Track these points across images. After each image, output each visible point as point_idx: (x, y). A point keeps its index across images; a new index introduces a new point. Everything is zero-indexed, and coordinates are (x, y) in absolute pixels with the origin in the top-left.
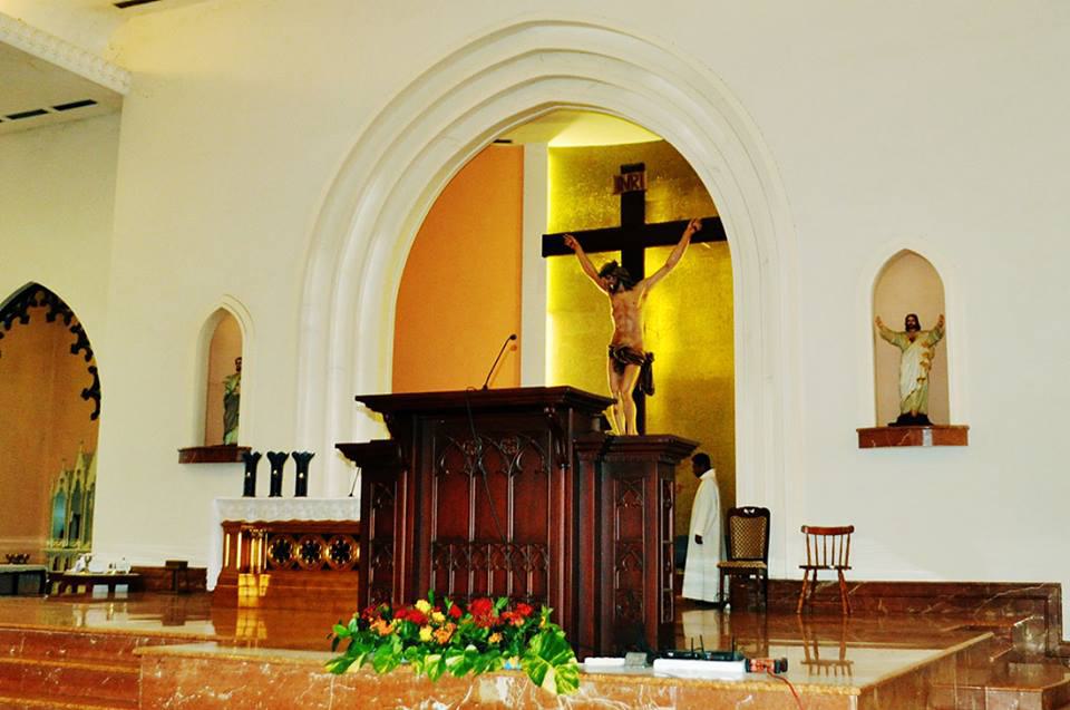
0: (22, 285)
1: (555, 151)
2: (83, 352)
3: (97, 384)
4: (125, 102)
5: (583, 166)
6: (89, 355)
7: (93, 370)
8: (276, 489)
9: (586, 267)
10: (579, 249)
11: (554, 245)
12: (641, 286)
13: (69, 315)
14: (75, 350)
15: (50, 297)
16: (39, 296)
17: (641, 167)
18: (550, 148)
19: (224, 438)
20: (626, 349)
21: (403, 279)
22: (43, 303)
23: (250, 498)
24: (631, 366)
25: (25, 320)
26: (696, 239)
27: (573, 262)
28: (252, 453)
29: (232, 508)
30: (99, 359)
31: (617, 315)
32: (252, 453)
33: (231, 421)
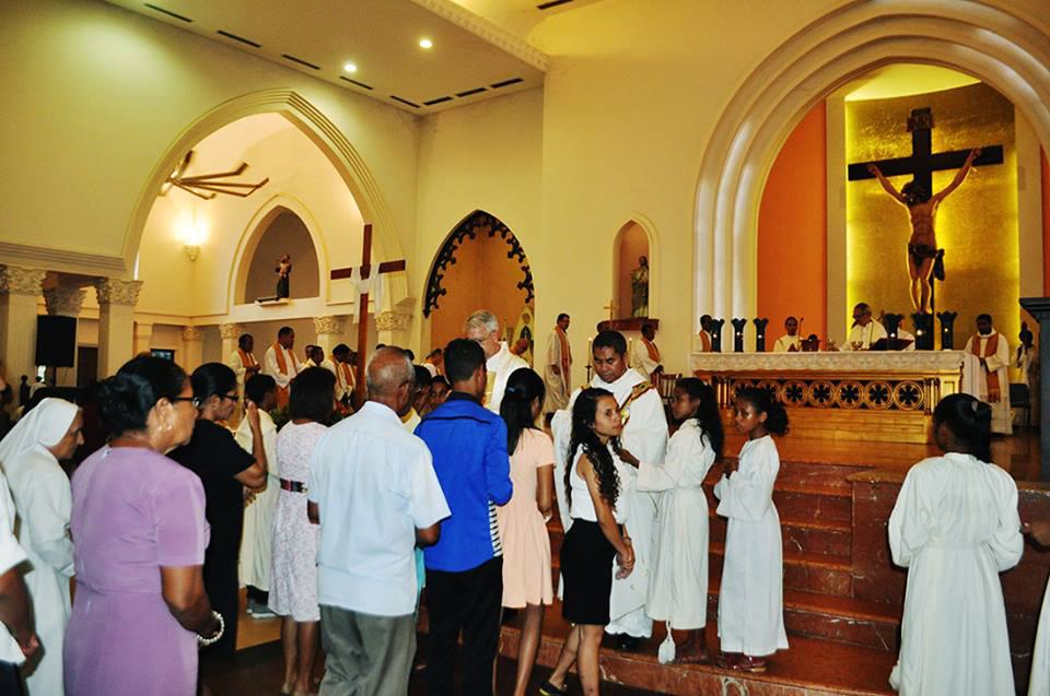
0: (468, 213)
1: (851, 103)
2: (517, 257)
3: (529, 277)
4: (546, 77)
5: (877, 117)
6: (522, 258)
7: (526, 269)
8: (739, 346)
9: (890, 189)
10: (881, 175)
11: (859, 172)
12: (931, 201)
13: (505, 231)
14: (510, 255)
15: (490, 220)
16: (482, 219)
17: (928, 110)
18: (848, 102)
19: (633, 313)
20: (924, 247)
21: (765, 193)
22: (486, 224)
23: (740, 353)
24: (927, 260)
25: (472, 237)
26: (975, 164)
27: (875, 188)
28: (415, 419)
29: (705, 360)
30: (530, 260)
31: (916, 221)
32: (415, 419)
33: (643, 299)
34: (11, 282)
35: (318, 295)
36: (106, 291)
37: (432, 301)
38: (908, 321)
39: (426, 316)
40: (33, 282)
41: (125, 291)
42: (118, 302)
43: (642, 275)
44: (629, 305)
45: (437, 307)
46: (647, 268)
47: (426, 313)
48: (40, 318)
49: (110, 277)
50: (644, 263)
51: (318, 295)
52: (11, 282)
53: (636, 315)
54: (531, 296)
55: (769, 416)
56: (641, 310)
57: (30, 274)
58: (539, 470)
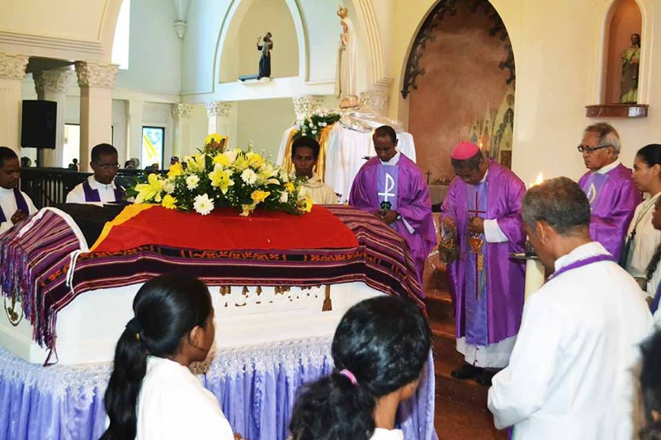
32: (212, 200)
34: (89, 76)
35: (298, 75)
36: (85, 75)
37: (410, 81)
38: (448, 218)
39: (405, 97)
40: (17, 67)
41: (103, 75)
42: (98, 85)
43: (634, 55)
44: (617, 88)
45: (415, 88)
46: (639, 46)
47: (404, 93)
48: (26, 104)
49: (88, 62)
50: (637, 41)
51: (298, 75)
52: (89, 76)
53: (624, 100)
54: (513, 77)
55: (656, 410)
56: (630, 94)
57: (15, 59)
58: (230, 293)
